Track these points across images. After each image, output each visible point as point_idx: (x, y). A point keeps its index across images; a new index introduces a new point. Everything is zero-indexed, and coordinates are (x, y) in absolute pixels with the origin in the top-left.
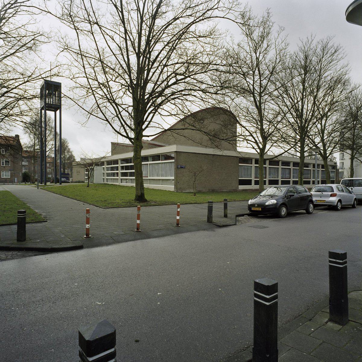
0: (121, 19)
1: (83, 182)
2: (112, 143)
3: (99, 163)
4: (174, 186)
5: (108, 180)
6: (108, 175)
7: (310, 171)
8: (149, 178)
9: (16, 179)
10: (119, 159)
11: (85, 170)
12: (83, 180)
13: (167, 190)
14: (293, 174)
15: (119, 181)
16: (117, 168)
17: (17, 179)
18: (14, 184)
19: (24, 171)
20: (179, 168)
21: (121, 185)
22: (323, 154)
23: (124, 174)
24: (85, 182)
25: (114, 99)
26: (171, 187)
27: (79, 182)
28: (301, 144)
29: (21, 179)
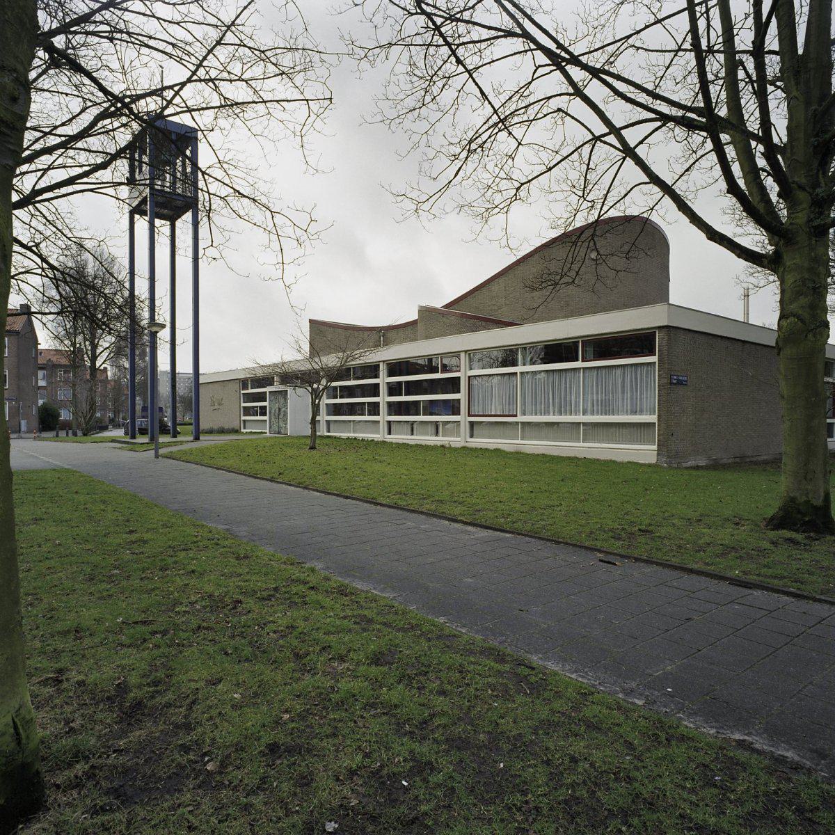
0: (733, 188)
1: (236, 431)
2: (311, 321)
3: (290, 377)
4: (655, 447)
5: (331, 426)
6: (247, 411)
7: (475, 382)
8: (520, 418)
9: (23, 423)
10: (384, 361)
11: (241, 395)
12: (235, 425)
13: (603, 457)
14: (641, 412)
15: (383, 427)
16: (374, 390)
17: (28, 423)
18: (21, 438)
19: (41, 402)
20: (672, 384)
21: (391, 440)
22: (190, 148)
23: (396, 409)
24: (242, 430)
25: (37, 205)
26: (646, 452)
27: (222, 431)
28: (829, 237)
29: (35, 423)
